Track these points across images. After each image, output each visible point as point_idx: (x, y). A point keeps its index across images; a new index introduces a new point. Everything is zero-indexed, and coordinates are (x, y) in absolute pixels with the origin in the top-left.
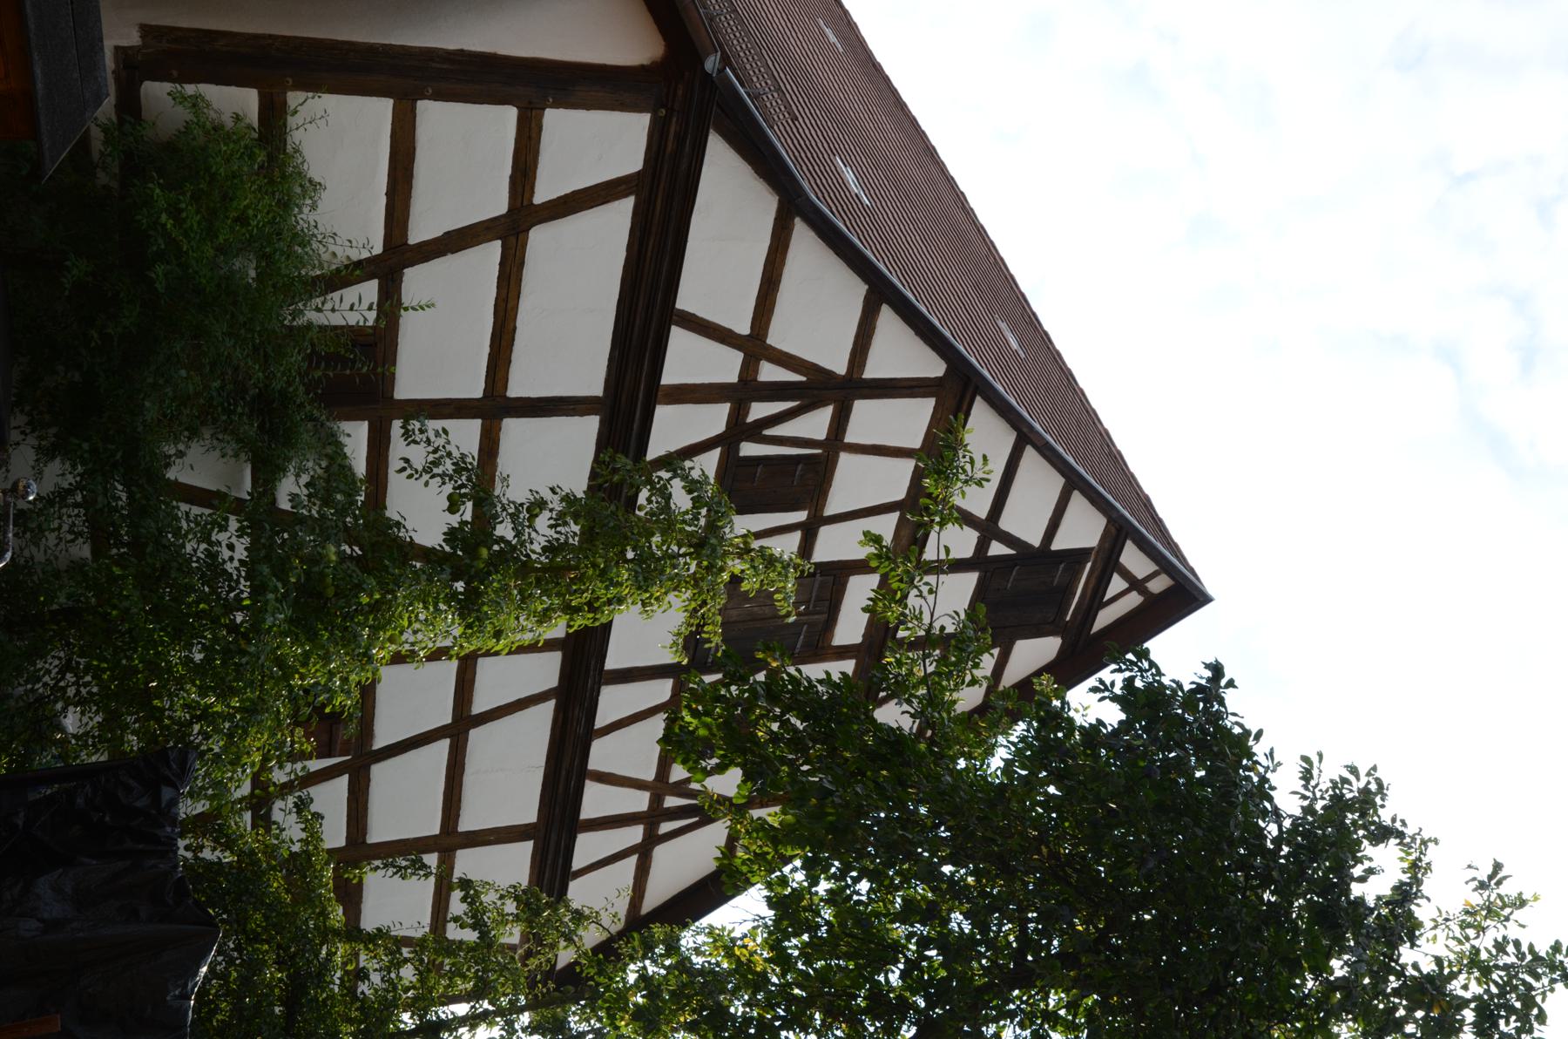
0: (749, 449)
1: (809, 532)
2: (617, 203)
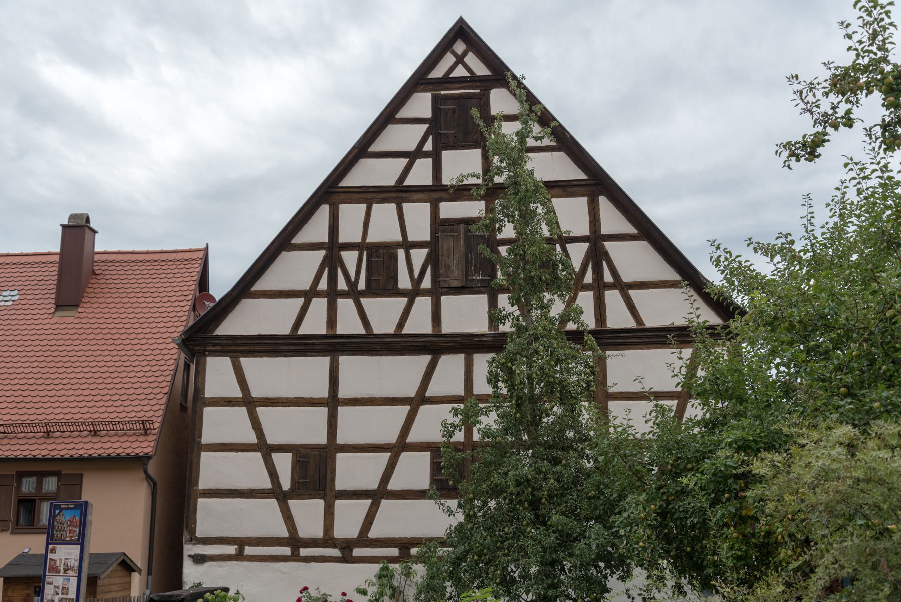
0: (362, 286)
1: (409, 246)
2: (242, 365)
